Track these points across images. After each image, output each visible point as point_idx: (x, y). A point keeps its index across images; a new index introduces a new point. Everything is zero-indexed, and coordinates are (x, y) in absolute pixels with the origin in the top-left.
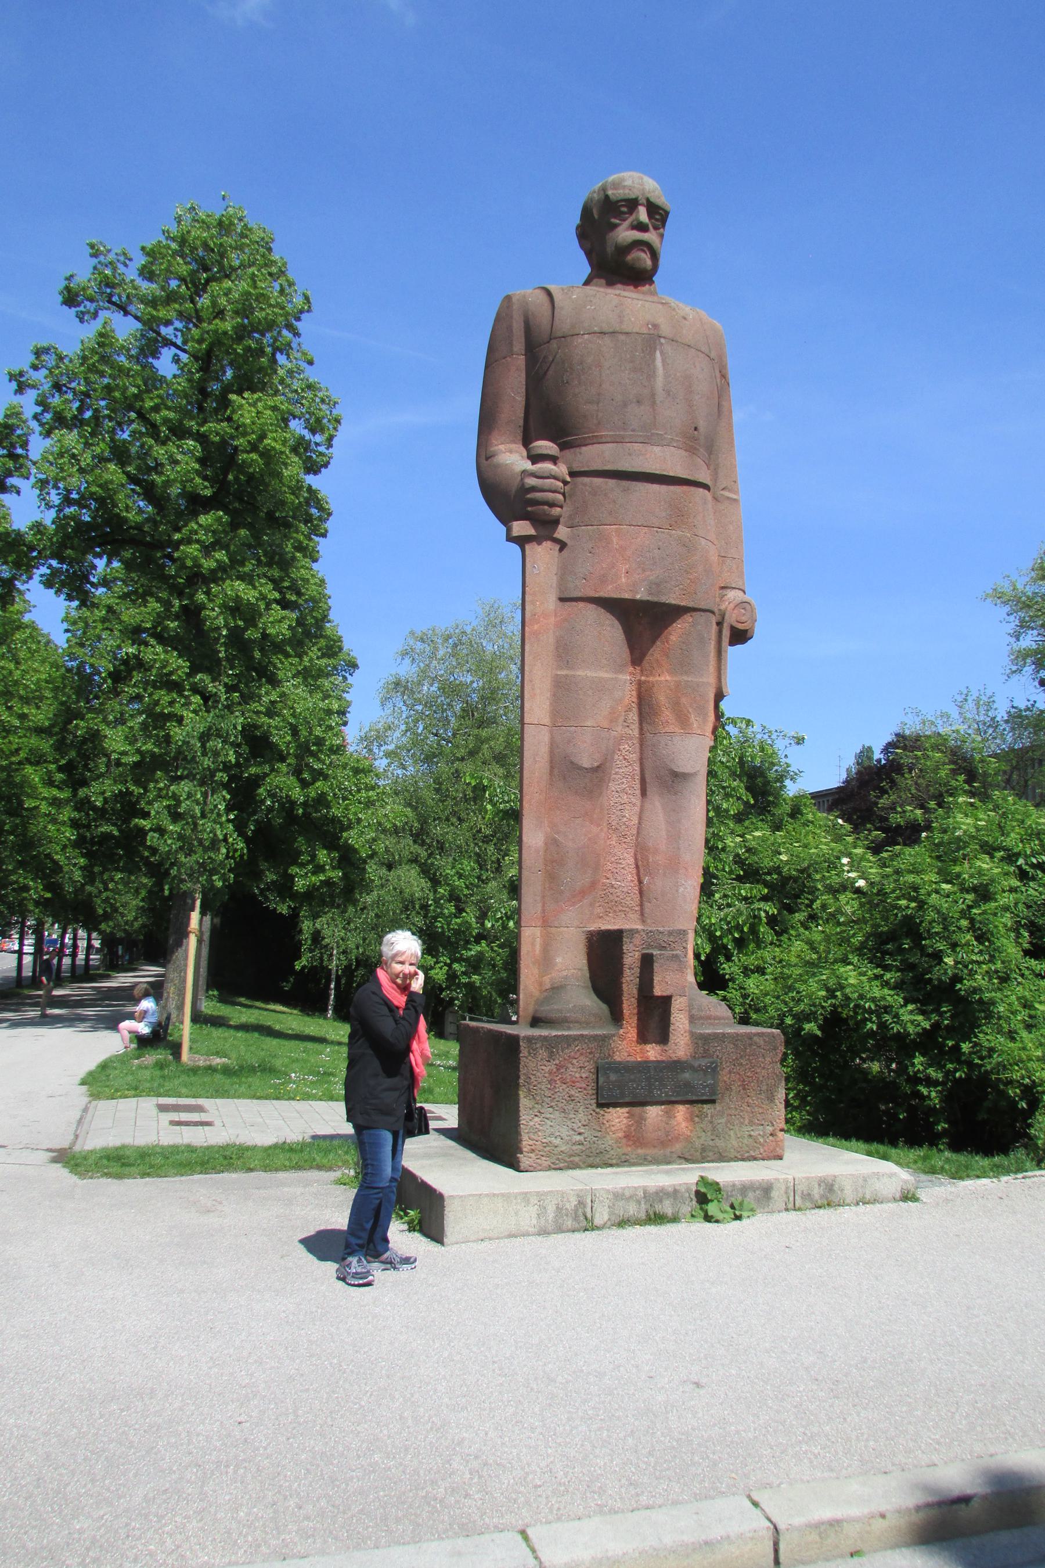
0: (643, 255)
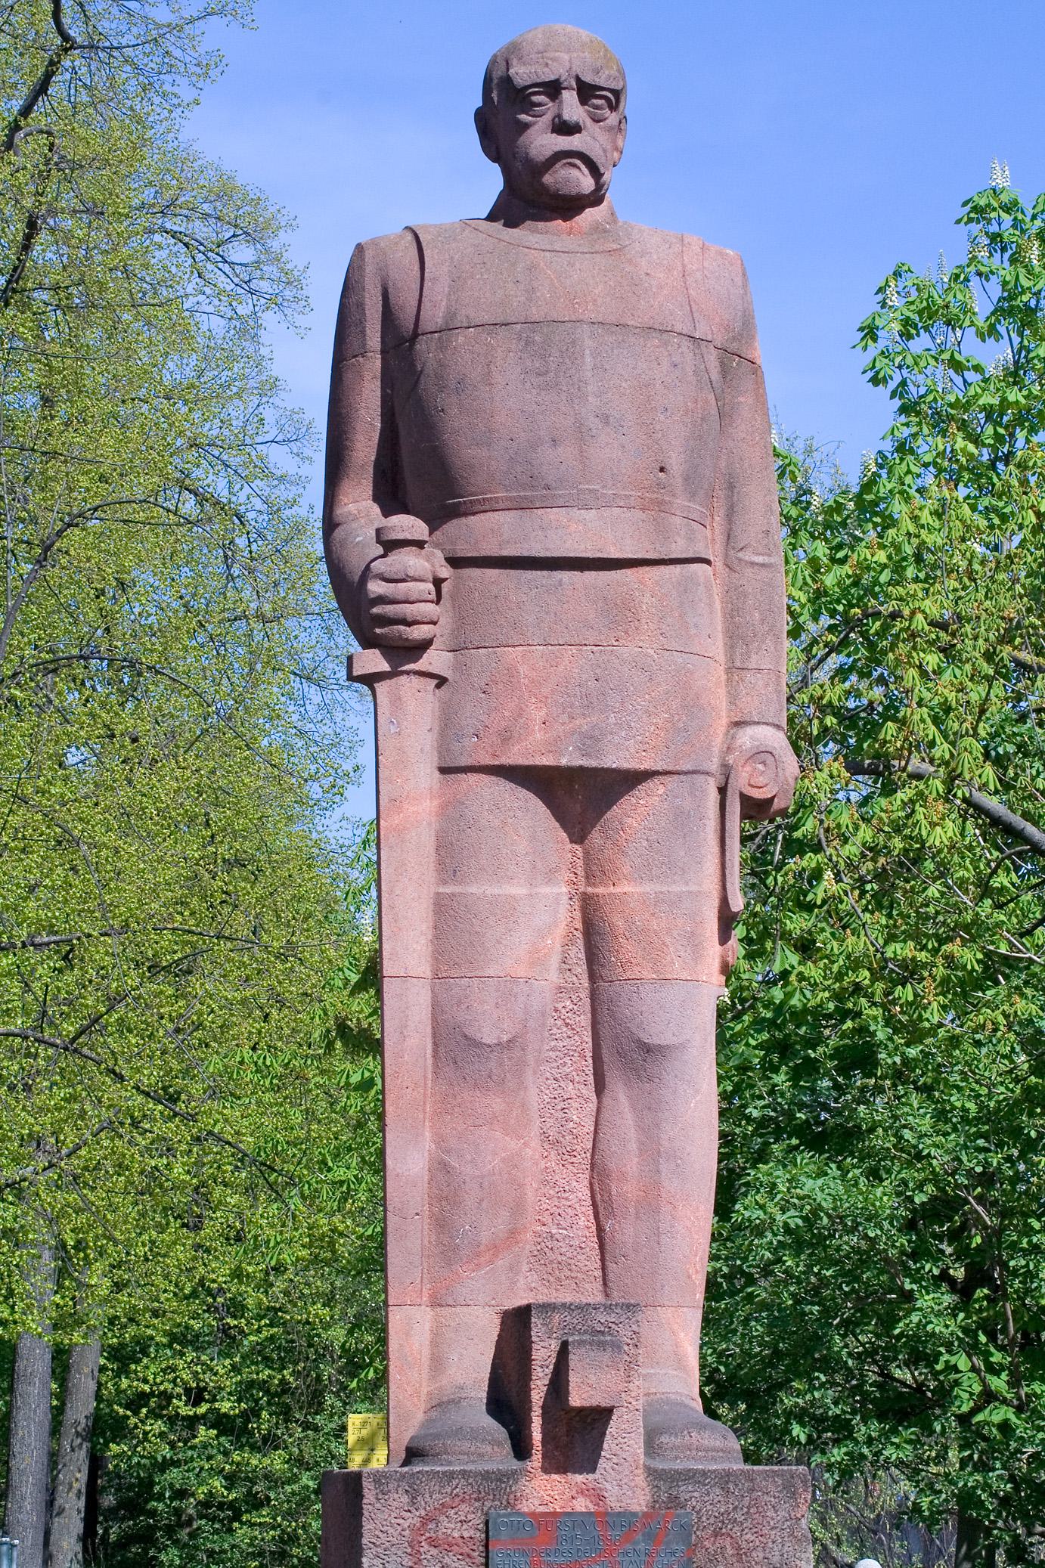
0: (574, 172)
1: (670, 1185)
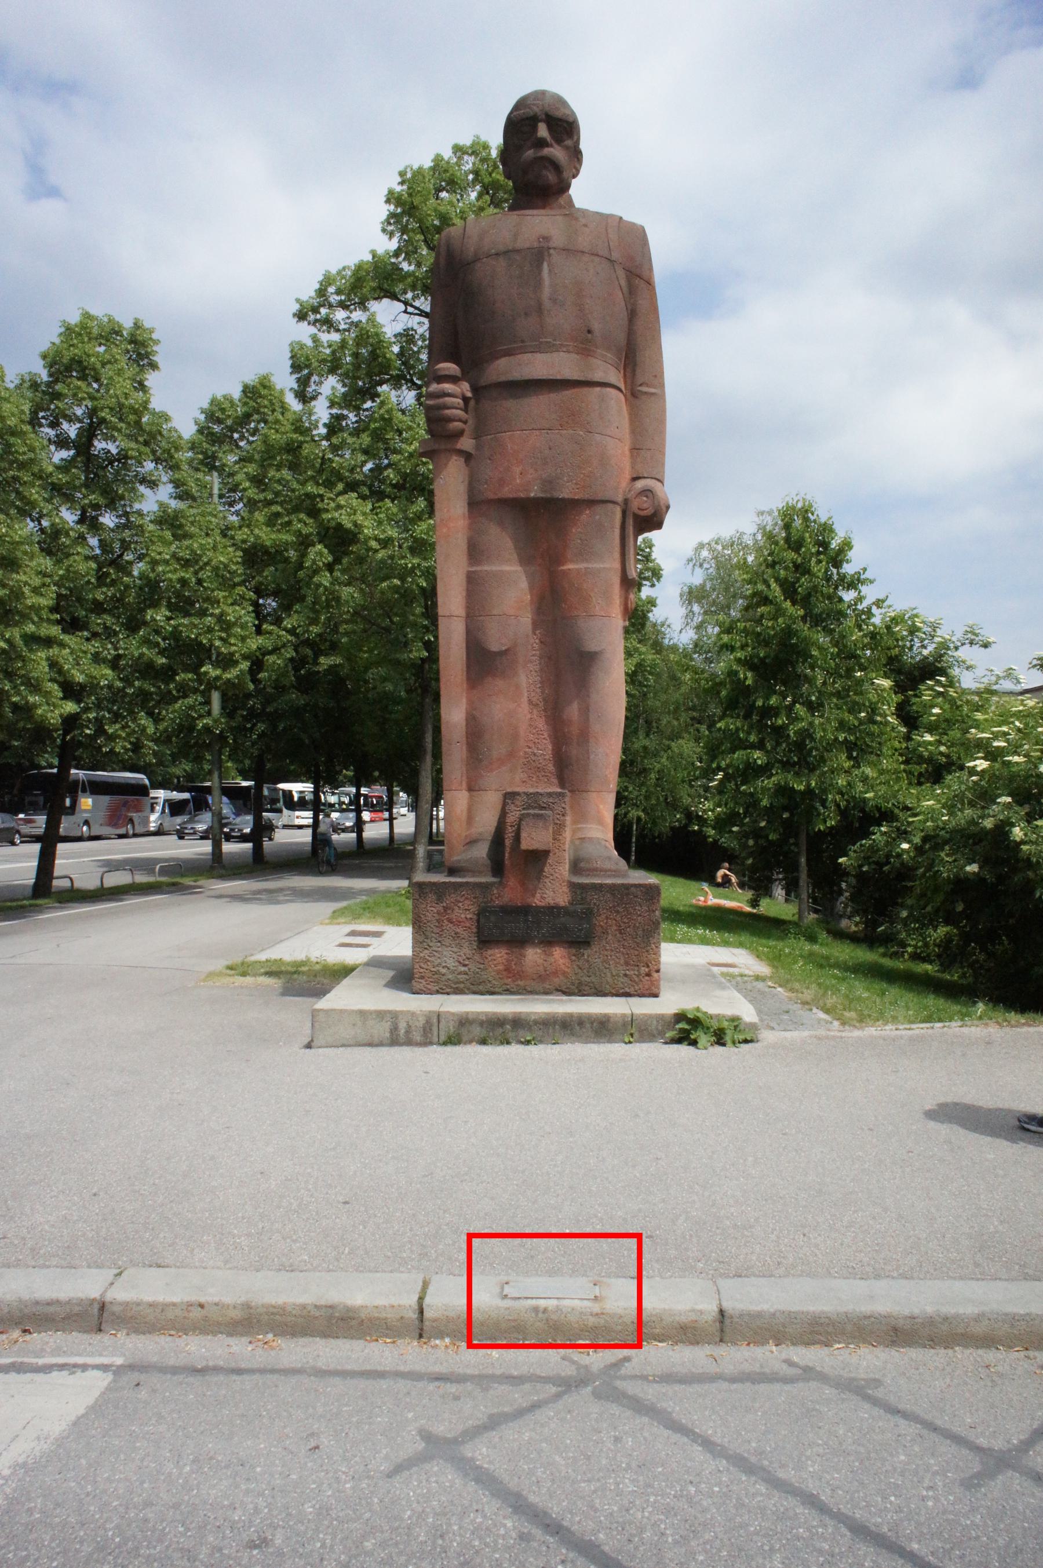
1: (595, 727)
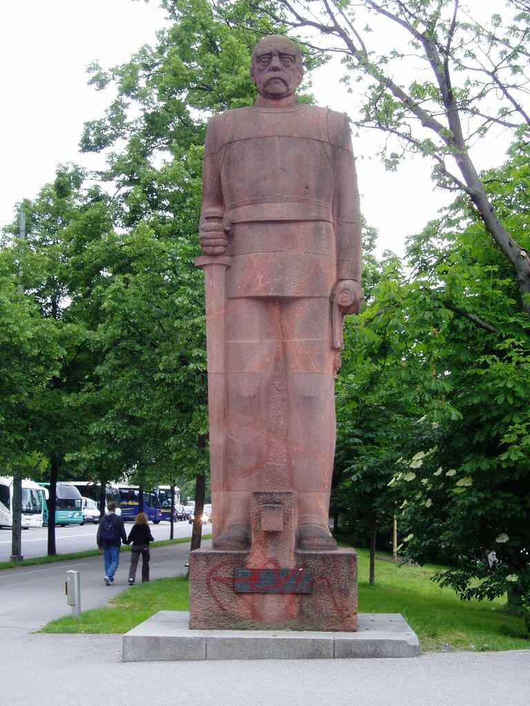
0: (278, 85)
